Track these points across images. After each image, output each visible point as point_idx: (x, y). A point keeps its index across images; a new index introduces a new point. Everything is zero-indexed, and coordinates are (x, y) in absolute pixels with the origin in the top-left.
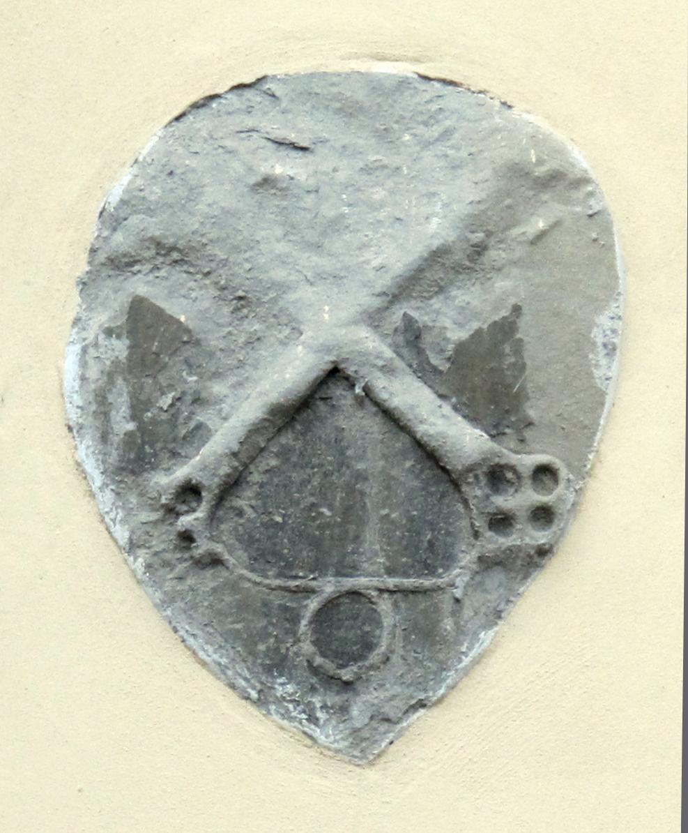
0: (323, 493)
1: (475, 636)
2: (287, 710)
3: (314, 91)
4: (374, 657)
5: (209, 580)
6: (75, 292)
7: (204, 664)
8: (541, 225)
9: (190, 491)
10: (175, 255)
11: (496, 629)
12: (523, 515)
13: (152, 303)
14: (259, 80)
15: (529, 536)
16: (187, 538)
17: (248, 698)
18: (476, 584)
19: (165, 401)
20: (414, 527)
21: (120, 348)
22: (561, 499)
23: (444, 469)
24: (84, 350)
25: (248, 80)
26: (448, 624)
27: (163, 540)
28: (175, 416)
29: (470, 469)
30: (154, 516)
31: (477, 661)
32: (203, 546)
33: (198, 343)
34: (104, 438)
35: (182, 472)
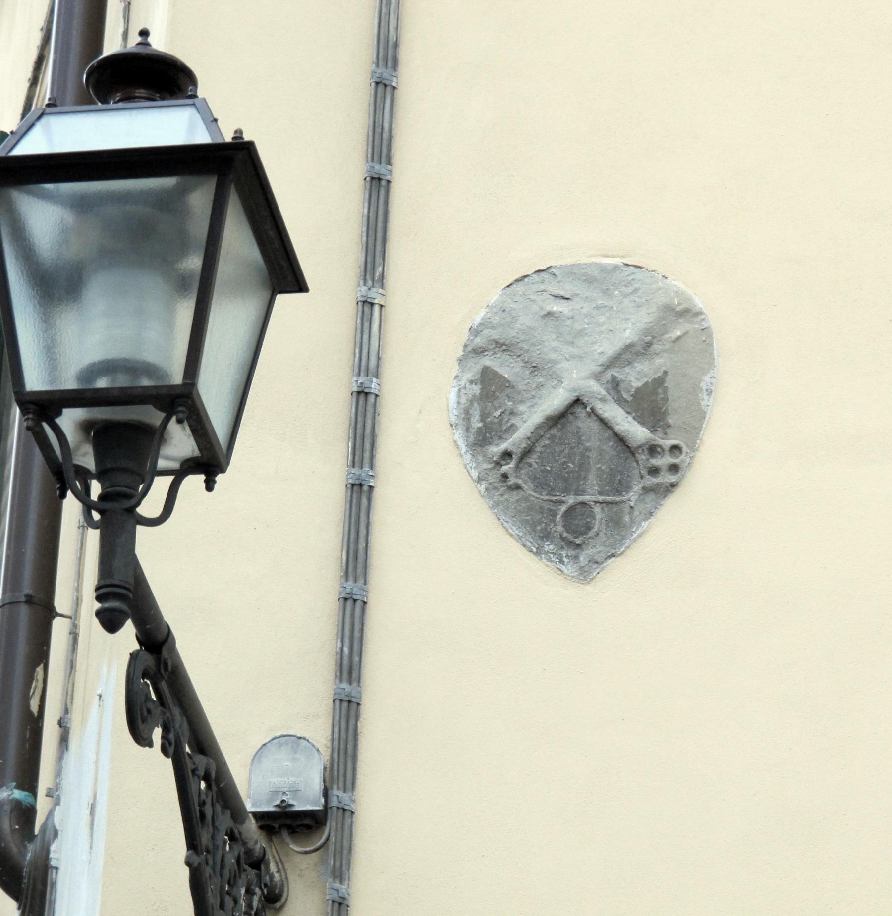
3: (574, 272)
4: (591, 533)
5: (515, 496)
7: (511, 535)
8: (679, 333)
10: (504, 347)
12: (664, 468)
16: (505, 476)
17: (531, 552)
18: (640, 500)
19: (497, 413)
20: (612, 473)
21: (476, 389)
23: (628, 446)
24: (459, 390)
26: (627, 518)
27: (494, 477)
28: (501, 420)
29: (640, 446)
31: (640, 536)
32: (512, 480)
33: (513, 387)
34: (468, 430)
35: (503, 446)
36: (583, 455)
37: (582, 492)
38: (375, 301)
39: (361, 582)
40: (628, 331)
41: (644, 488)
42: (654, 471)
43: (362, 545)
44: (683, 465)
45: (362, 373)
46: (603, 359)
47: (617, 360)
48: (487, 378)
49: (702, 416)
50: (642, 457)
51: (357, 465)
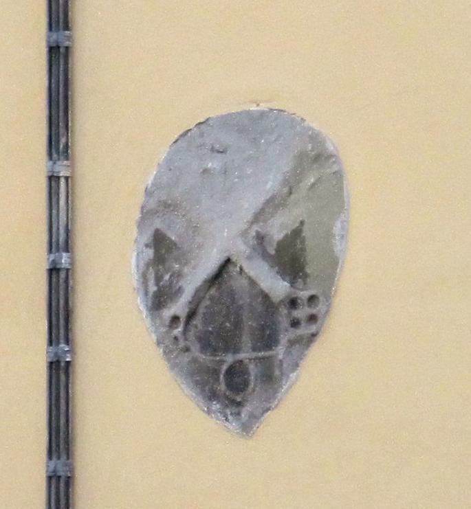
0: (227, 316)
1: (288, 376)
2: (218, 416)
3: (227, 122)
5: (186, 358)
8: (312, 180)
9: (175, 319)
11: (298, 371)
12: (303, 324)
13: (218, 117)
14: (207, 120)
17: (204, 411)
18: (288, 353)
20: (262, 328)
21: (150, 253)
22: (319, 311)
24: (138, 254)
25: (202, 120)
26: (277, 373)
29: (282, 301)
31: (290, 387)
34: (146, 293)
37: (236, 350)
38: (61, 175)
39: (64, 457)
40: (270, 183)
41: (289, 341)
42: (295, 324)
43: (62, 421)
44: (320, 316)
45: (53, 29)
47: (258, 217)
50: (284, 311)
51: (53, 250)
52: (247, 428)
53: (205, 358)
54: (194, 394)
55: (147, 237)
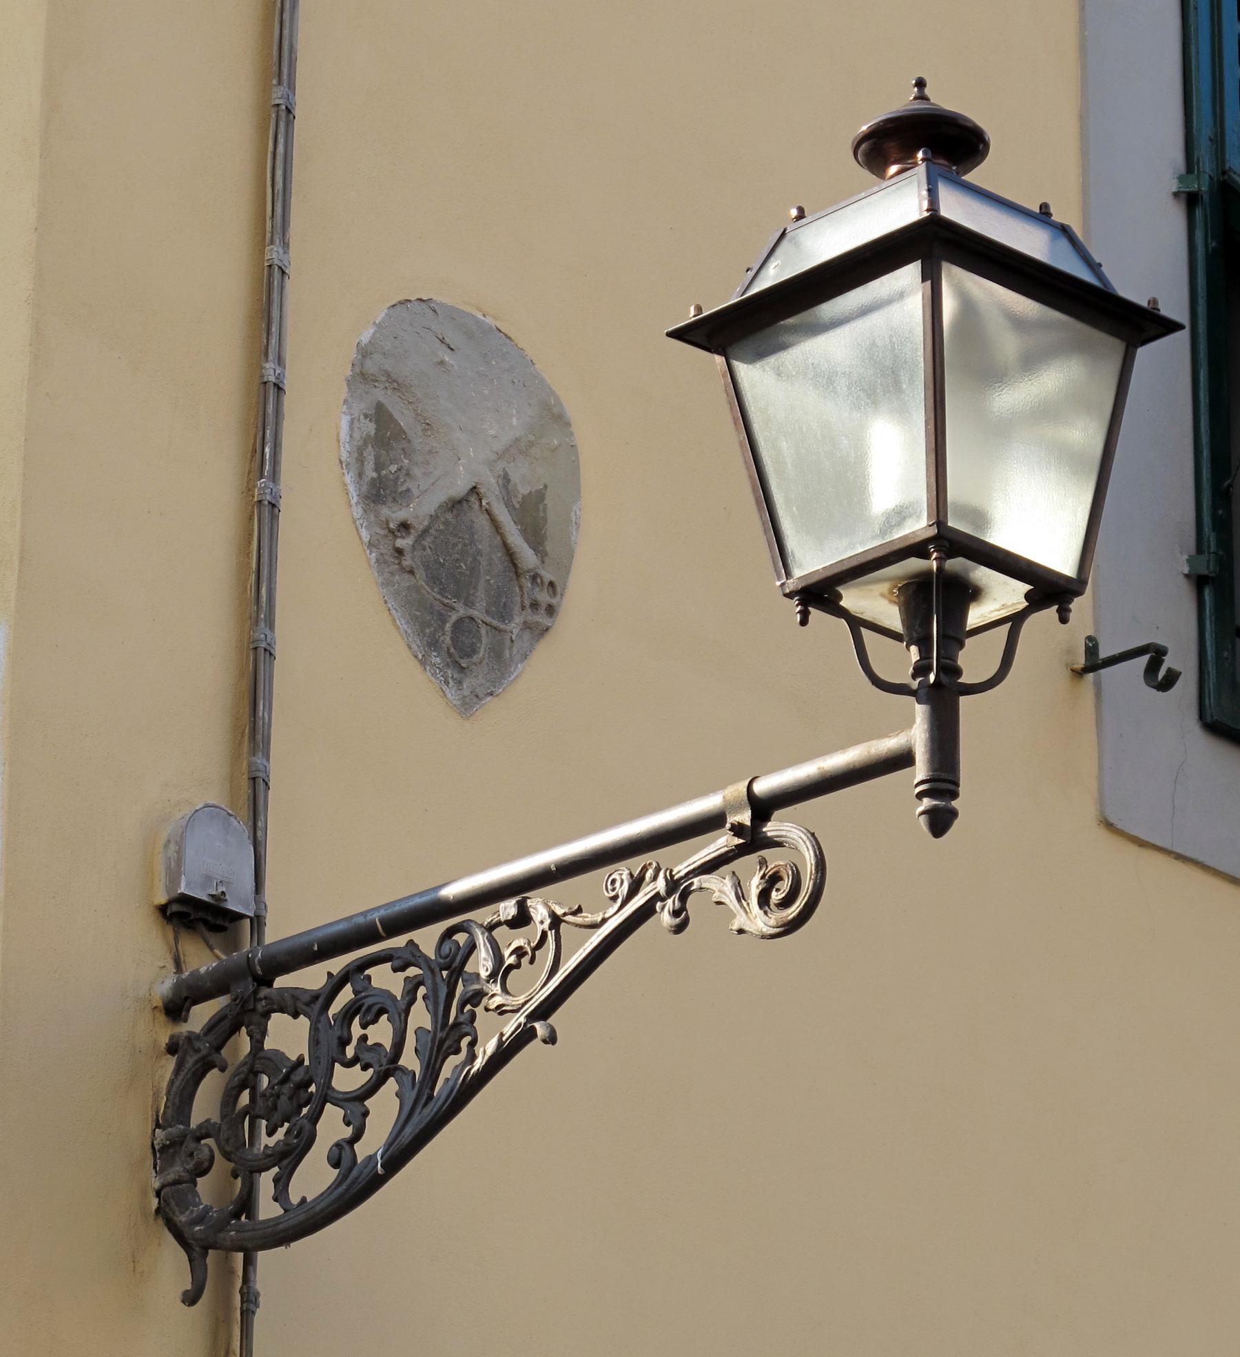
1: (516, 667)
3: (454, 315)
4: (475, 658)
5: (406, 580)
6: (345, 384)
7: (398, 628)
9: (405, 526)
10: (395, 385)
15: (541, 618)
16: (400, 552)
17: (416, 657)
19: (393, 468)
23: (515, 566)
24: (352, 420)
27: (386, 548)
28: (397, 479)
30: (383, 532)
31: (517, 677)
32: (407, 562)
33: (409, 441)
34: (360, 475)
35: (402, 514)
36: (475, 559)
46: (498, 446)
48: (380, 415)
49: (571, 555)
52: (468, 705)
53: (432, 594)
54: (409, 631)
55: (360, 407)
